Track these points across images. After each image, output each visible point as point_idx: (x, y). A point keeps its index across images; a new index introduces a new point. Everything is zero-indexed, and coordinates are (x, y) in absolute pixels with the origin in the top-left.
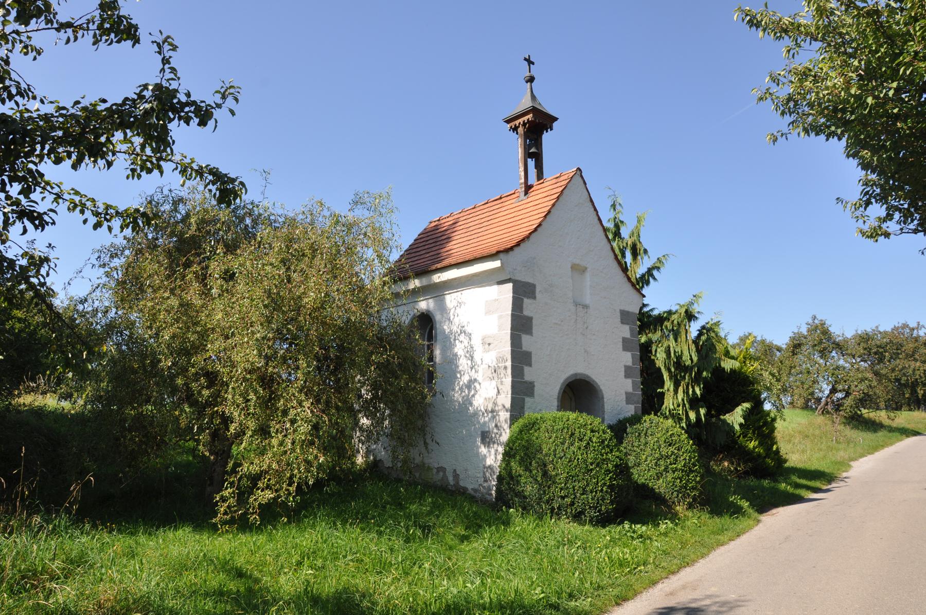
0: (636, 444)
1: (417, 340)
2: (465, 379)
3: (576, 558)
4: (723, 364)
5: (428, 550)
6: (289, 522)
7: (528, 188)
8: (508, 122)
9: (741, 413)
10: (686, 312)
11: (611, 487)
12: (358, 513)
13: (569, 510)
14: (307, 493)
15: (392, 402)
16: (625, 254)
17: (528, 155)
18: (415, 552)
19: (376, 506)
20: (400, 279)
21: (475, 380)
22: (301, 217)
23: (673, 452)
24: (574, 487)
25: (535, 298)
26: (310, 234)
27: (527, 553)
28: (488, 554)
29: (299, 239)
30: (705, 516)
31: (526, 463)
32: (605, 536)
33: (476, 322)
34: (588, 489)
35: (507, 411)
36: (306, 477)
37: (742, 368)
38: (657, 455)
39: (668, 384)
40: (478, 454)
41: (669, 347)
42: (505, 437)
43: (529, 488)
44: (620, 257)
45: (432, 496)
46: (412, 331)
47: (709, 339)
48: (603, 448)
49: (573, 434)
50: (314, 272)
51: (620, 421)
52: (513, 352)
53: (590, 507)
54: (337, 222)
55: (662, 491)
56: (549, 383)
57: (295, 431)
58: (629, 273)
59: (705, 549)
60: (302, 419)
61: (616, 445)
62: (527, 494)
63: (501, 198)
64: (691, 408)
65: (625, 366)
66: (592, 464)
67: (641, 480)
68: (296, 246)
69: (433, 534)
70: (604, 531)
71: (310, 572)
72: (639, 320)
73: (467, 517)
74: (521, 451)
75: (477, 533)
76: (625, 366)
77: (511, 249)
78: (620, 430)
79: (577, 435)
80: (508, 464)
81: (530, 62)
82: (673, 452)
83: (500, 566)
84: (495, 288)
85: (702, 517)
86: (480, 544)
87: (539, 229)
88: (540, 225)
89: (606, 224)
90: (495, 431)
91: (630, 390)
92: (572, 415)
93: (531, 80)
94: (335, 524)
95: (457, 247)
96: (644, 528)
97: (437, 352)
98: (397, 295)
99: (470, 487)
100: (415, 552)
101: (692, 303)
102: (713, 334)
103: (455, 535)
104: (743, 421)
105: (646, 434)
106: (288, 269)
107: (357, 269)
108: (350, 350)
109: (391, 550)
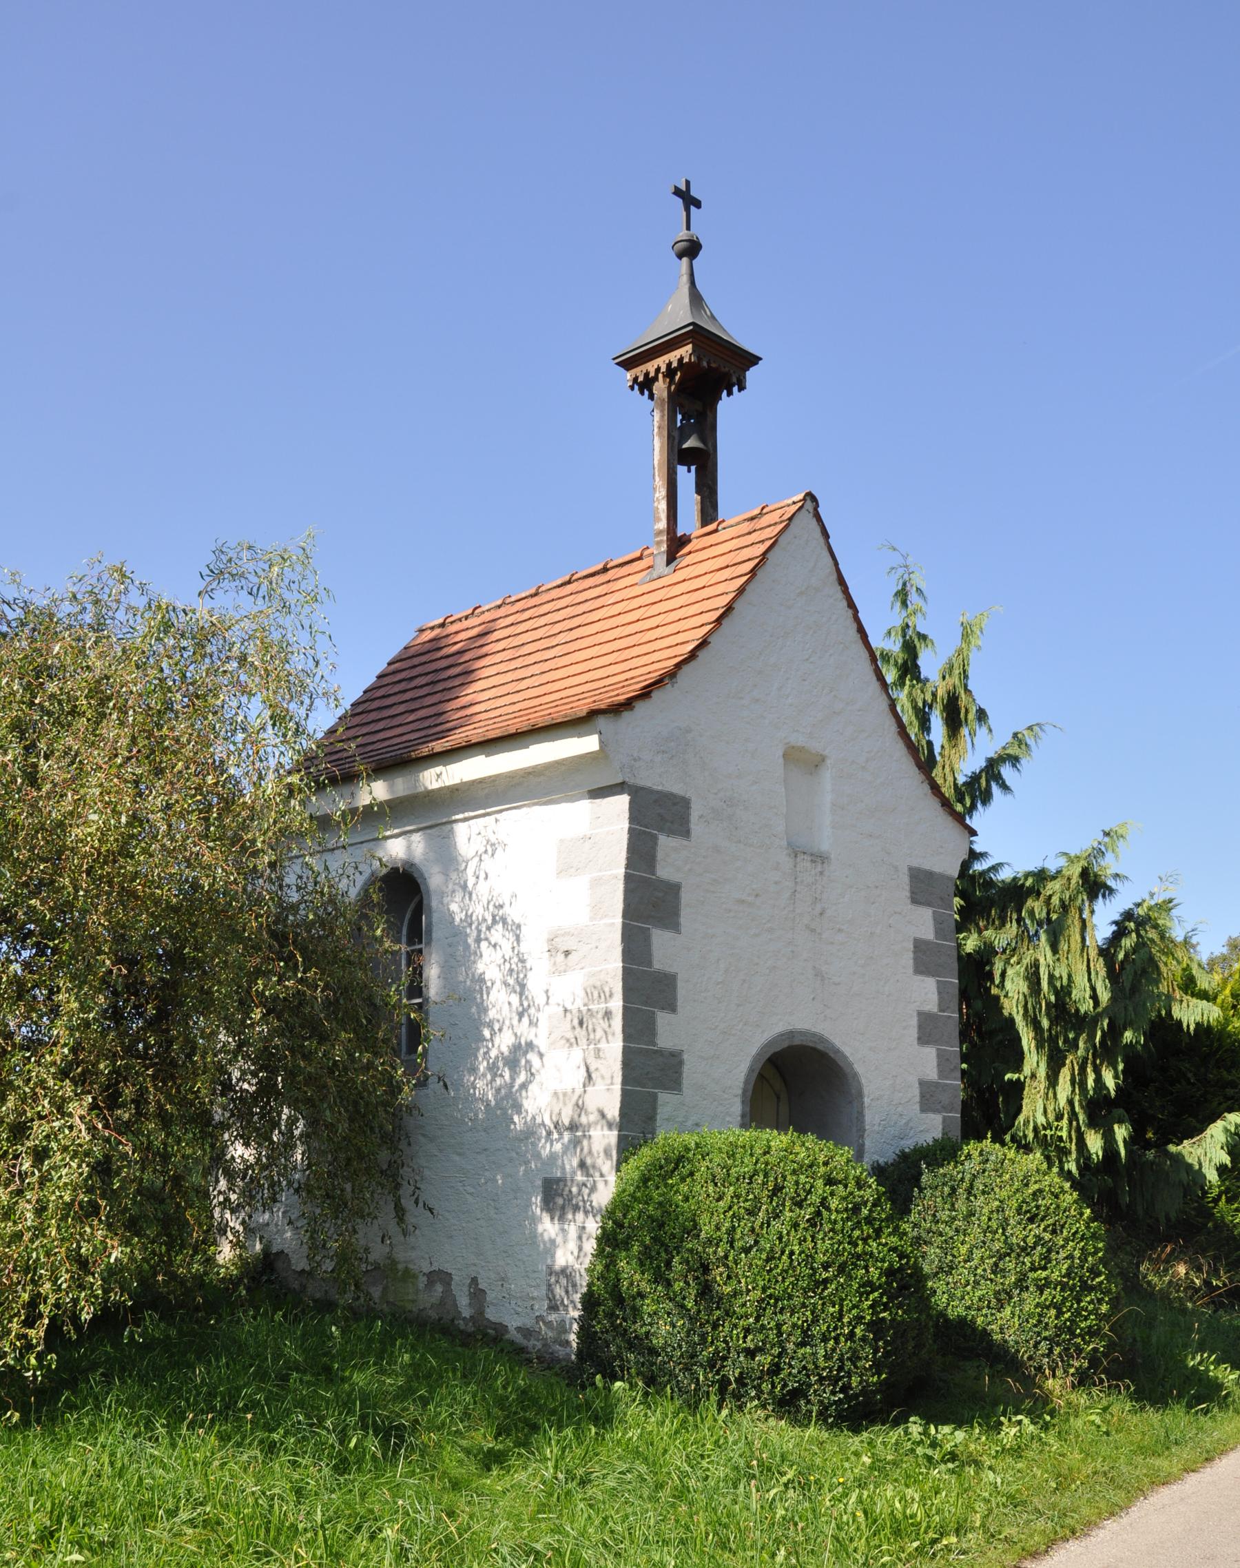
0: (944, 1215)
1: (380, 941)
2: (504, 1042)
3: (780, 1512)
4: (1177, 1012)
5: (396, 1490)
6: (25, 1423)
7: (676, 544)
8: (628, 364)
9: (1222, 1138)
10: (1085, 873)
11: (876, 1327)
12: (212, 1395)
13: (766, 1387)
14: (79, 1343)
15: (309, 1101)
16: (926, 710)
17: (679, 456)
18: (363, 1495)
19: (262, 1376)
20: (334, 781)
21: (530, 1045)
22: (67, 608)
23: (1039, 1238)
24: (779, 1326)
25: (686, 834)
26: (92, 654)
27: (653, 1499)
28: (554, 1500)
29: (63, 668)
30: (1122, 1406)
31: (656, 1264)
32: (857, 1454)
33: (534, 896)
34: (815, 1331)
35: (610, 1126)
36: (75, 1301)
37: (1227, 1020)
38: (997, 1246)
39: (1034, 1062)
40: (534, 1237)
41: (1036, 965)
42: (604, 1195)
43: (664, 1329)
44: (913, 732)
45: (414, 1349)
46: (365, 916)
47: (1141, 945)
48: (858, 1225)
49: (777, 1189)
50: (98, 756)
51: (903, 1156)
52: (627, 974)
53: (821, 1379)
54: (167, 626)
55: (1011, 1339)
56: (720, 1054)
57: (44, 1180)
58: (937, 773)
59: (1120, 1493)
60: (65, 1149)
61: (889, 1219)
62: (657, 1342)
63: (605, 570)
64: (1093, 1123)
65: (920, 1014)
66: (826, 1266)
67: (956, 1310)
68: (52, 687)
69: (411, 1449)
70: (855, 1442)
71: (76, 1557)
72: (961, 893)
73: (501, 1402)
74: (646, 1230)
75: (525, 1444)
76: (920, 1014)
77: (628, 704)
78: (901, 1178)
79: (790, 1189)
80: (610, 1264)
81: (689, 200)
82: (1039, 1238)
83: (583, 1533)
84: (584, 808)
85: (1115, 1409)
86: (531, 1475)
87: (702, 654)
88: (704, 643)
89: (877, 642)
90: (580, 1177)
91: (932, 1074)
92: (779, 1140)
93: (691, 250)
94: (149, 1426)
95: (489, 698)
96: (960, 1435)
97: (433, 973)
98: (324, 822)
99: (513, 1323)
100: (363, 1495)
101: (1099, 853)
102: (1153, 934)
103: (468, 1452)
104: (1226, 1159)
105: (969, 1191)
106: (30, 749)
107: (219, 750)
108: (199, 964)
109: (299, 1492)
